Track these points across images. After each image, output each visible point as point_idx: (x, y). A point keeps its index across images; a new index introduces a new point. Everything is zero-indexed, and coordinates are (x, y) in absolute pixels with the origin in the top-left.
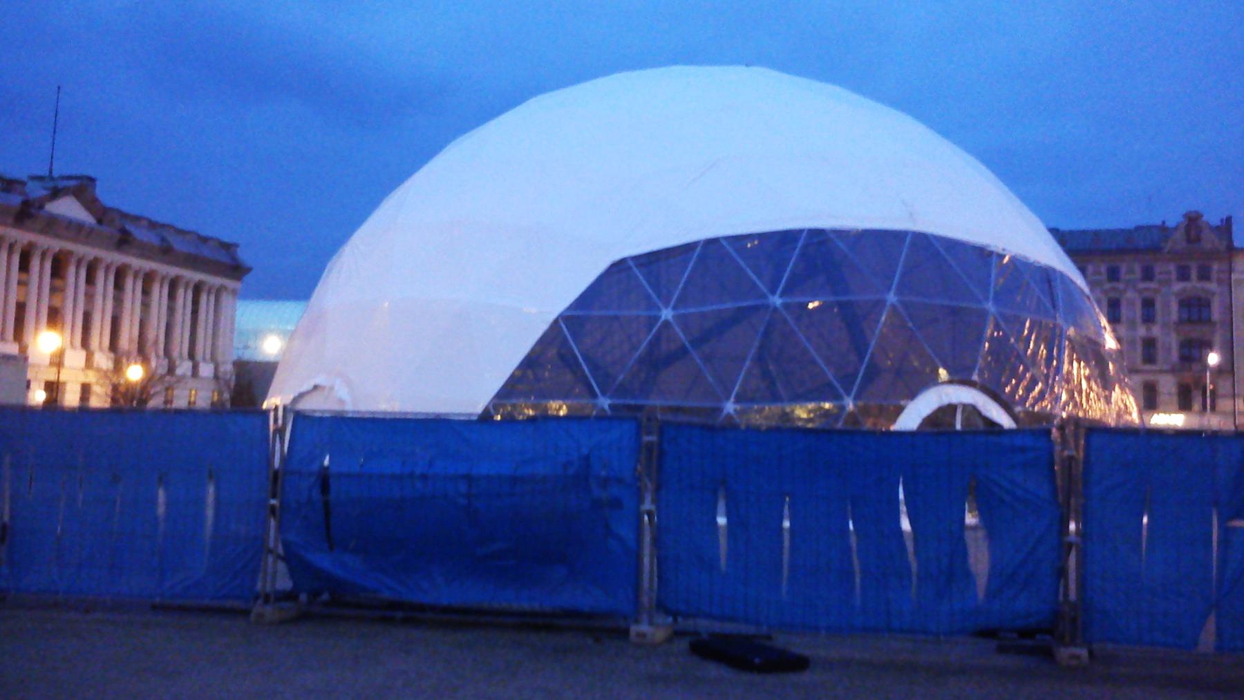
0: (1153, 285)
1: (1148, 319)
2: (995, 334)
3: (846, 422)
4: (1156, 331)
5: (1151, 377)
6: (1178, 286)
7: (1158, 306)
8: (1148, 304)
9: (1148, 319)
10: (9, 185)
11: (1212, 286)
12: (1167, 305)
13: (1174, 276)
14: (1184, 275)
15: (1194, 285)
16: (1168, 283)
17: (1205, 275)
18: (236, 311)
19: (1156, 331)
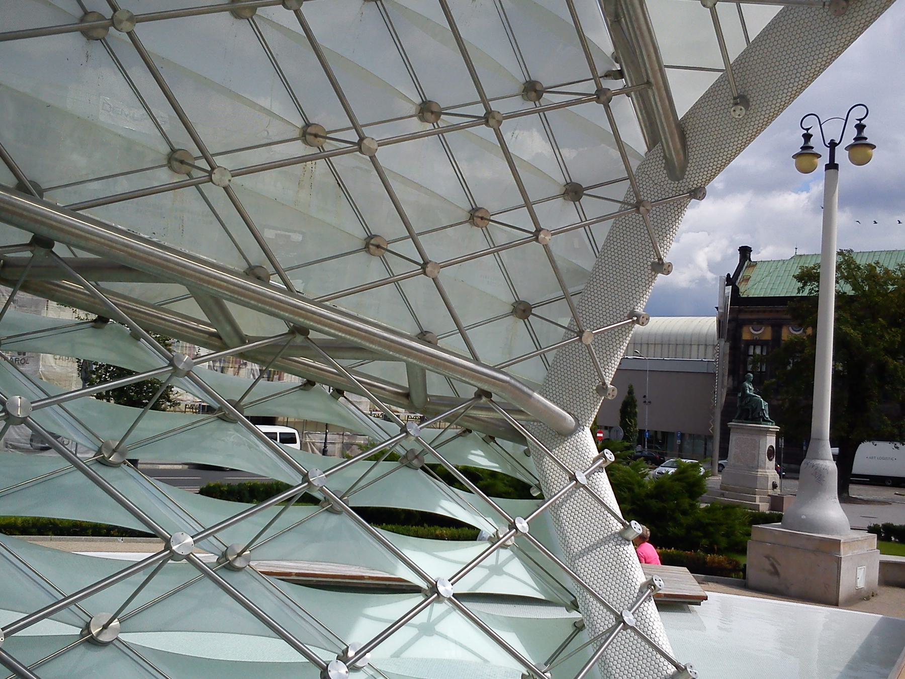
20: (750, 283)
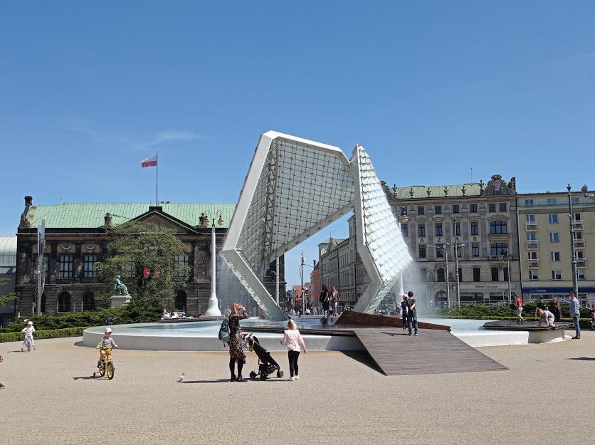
0: (476, 215)
1: (475, 233)
2: (259, 376)
3: (563, 304)
4: (479, 239)
5: (477, 264)
6: (489, 215)
7: (479, 225)
8: (474, 225)
9: (475, 233)
10: (586, 323)
11: (507, 214)
12: (484, 225)
13: (487, 210)
14: (492, 209)
15: (498, 213)
16: (484, 213)
17: (503, 209)
18: (47, 328)
19: (479, 239)
20: (34, 219)
